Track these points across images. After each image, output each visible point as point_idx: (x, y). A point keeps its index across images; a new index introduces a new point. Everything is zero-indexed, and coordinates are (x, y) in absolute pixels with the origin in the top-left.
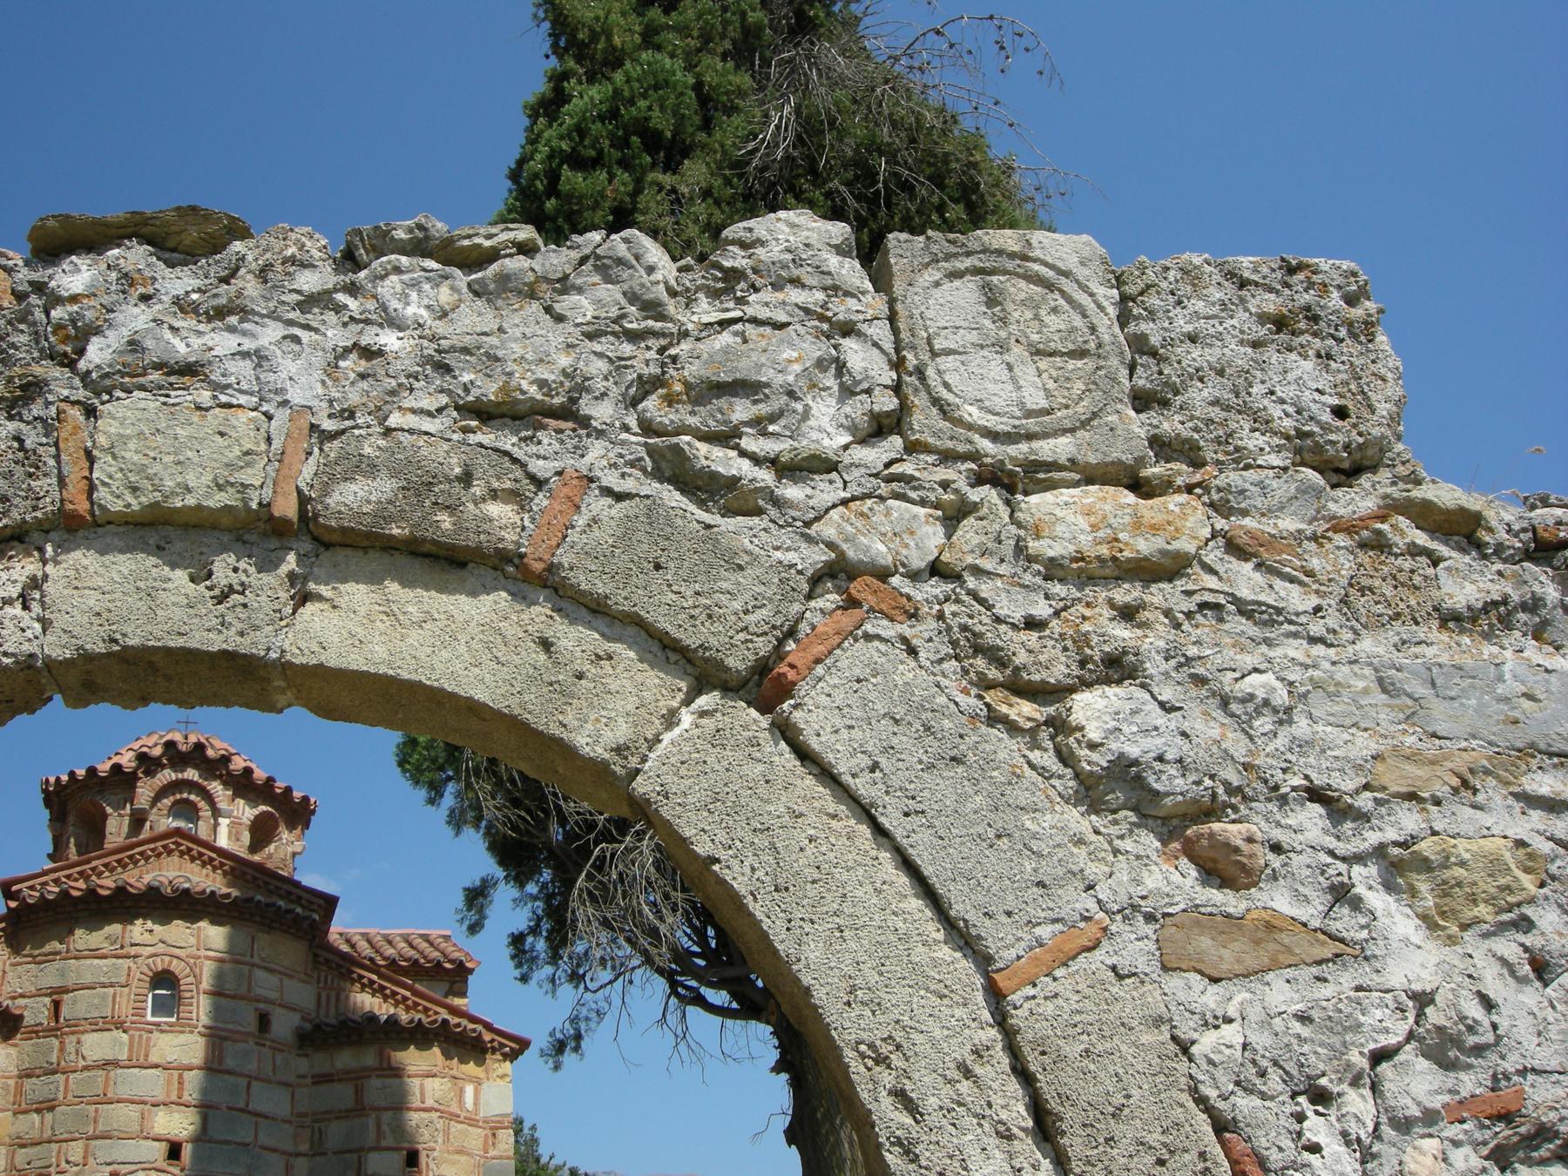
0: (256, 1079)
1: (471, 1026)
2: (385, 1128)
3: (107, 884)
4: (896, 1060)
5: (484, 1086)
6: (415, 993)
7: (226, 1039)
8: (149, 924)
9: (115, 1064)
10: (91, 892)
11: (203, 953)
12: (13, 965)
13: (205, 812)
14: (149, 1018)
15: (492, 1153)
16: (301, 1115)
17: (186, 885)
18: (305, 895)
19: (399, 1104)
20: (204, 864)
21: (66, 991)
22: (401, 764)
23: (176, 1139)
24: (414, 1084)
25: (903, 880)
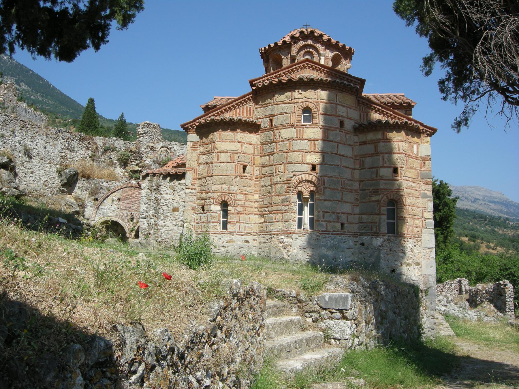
0: (340, 143)
1: (415, 124)
2: (385, 159)
3: (285, 79)
5: (420, 146)
6: (394, 113)
7: (329, 130)
8: (300, 91)
9: (292, 139)
10: (280, 82)
11: (319, 100)
12: (256, 108)
13: (316, 55)
14: (303, 123)
15: (423, 169)
16: (356, 156)
17: (312, 77)
18: (353, 79)
19: (390, 152)
20: (317, 71)
21: (274, 116)
22: (396, 11)
23: (314, 163)
24: (395, 145)
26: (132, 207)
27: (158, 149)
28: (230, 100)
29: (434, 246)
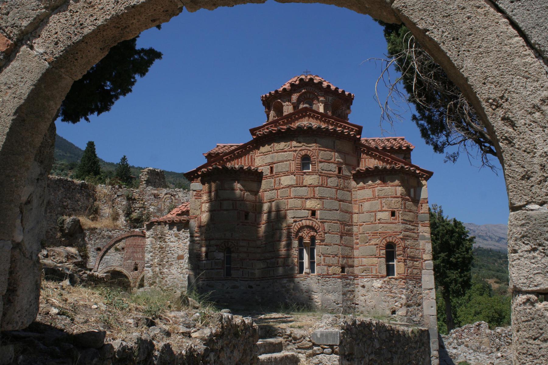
4: (505, 105)
25: (512, 30)
26: (136, 256)
27: (162, 196)
28: (233, 148)
29: (434, 287)
